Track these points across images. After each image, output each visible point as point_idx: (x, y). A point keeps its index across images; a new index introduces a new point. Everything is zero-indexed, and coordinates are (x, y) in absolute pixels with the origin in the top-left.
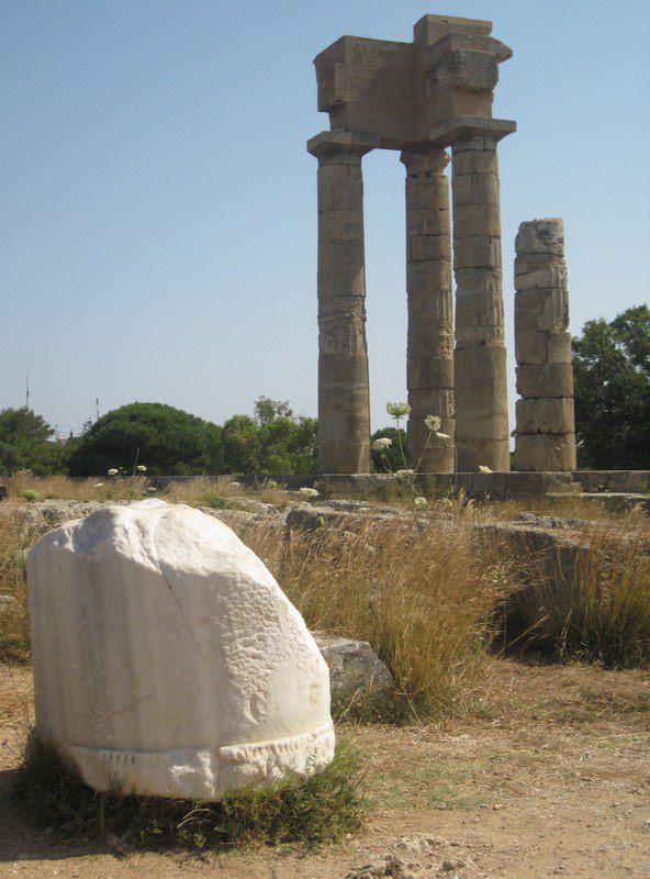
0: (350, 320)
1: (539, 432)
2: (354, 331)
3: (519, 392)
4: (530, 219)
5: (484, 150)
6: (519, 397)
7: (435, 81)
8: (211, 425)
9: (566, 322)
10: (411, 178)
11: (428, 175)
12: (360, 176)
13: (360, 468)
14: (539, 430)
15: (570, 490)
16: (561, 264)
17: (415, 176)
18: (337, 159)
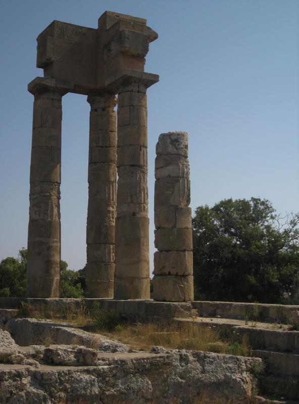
1: (169, 274)
3: (156, 246)
4: (166, 132)
5: (138, 92)
6: (156, 250)
7: (110, 50)
9: (188, 201)
10: (93, 111)
11: (103, 109)
12: (60, 107)
14: (169, 272)
15: (190, 316)
16: (186, 162)
18: (47, 95)
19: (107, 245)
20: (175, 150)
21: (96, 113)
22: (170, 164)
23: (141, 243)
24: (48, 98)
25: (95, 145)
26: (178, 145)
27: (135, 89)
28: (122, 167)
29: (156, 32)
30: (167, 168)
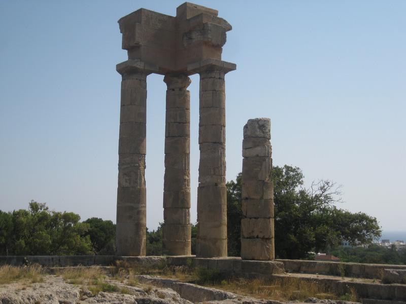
0: (138, 168)
1: (257, 237)
2: (140, 174)
4: (253, 118)
5: (219, 78)
7: (191, 38)
8: (5, 213)
11: (181, 89)
13: (141, 253)
17: (173, 90)
19: (184, 209)
20: (262, 134)
21: (173, 92)
22: (258, 146)
23: (222, 210)
24: (137, 79)
25: (173, 121)
26: (265, 130)
27: (217, 76)
28: (207, 144)
29: (231, 24)
30: (256, 149)
